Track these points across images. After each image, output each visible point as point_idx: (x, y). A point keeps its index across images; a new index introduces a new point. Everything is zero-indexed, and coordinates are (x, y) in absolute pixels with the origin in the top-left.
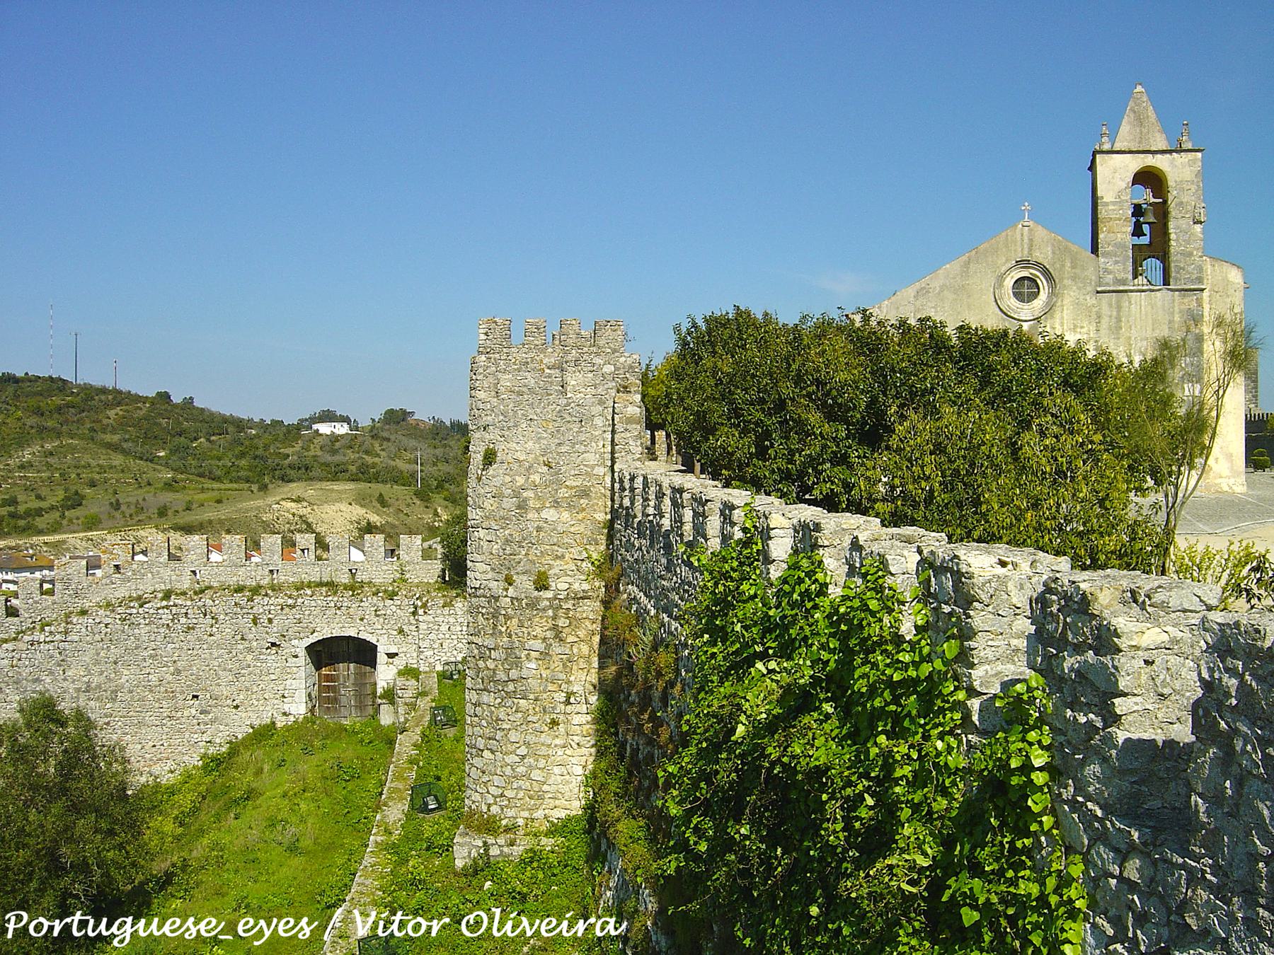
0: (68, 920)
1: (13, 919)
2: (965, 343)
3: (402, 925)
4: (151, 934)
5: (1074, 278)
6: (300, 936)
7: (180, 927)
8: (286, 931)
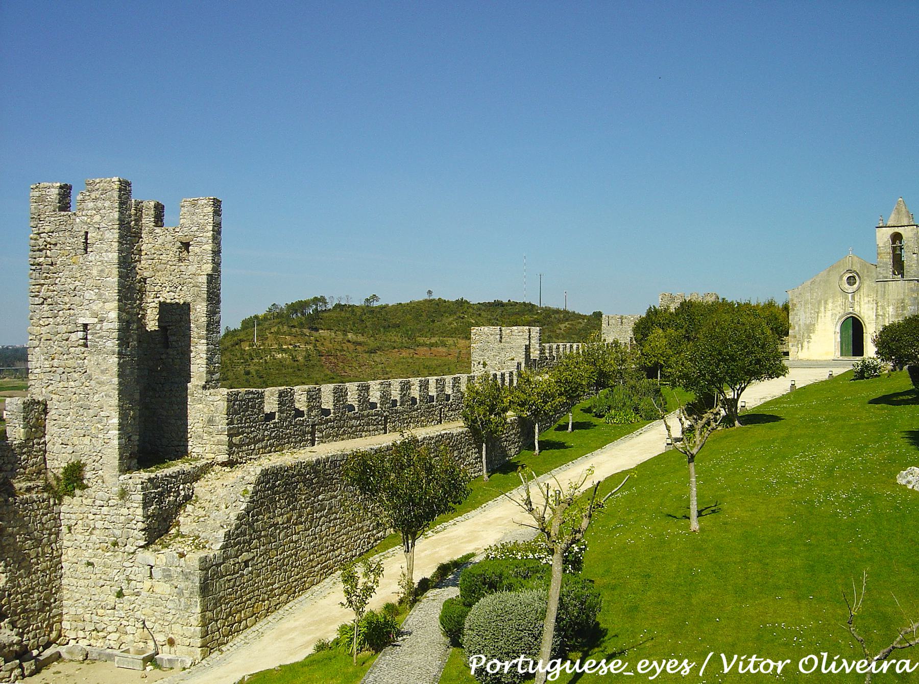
0: (515, 661)
1: (475, 661)
2: (225, 381)
3: (756, 666)
4: (830, 672)
5: (868, 276)
6: (600, 673)
7: (677, 667)
8: (672, 669)
